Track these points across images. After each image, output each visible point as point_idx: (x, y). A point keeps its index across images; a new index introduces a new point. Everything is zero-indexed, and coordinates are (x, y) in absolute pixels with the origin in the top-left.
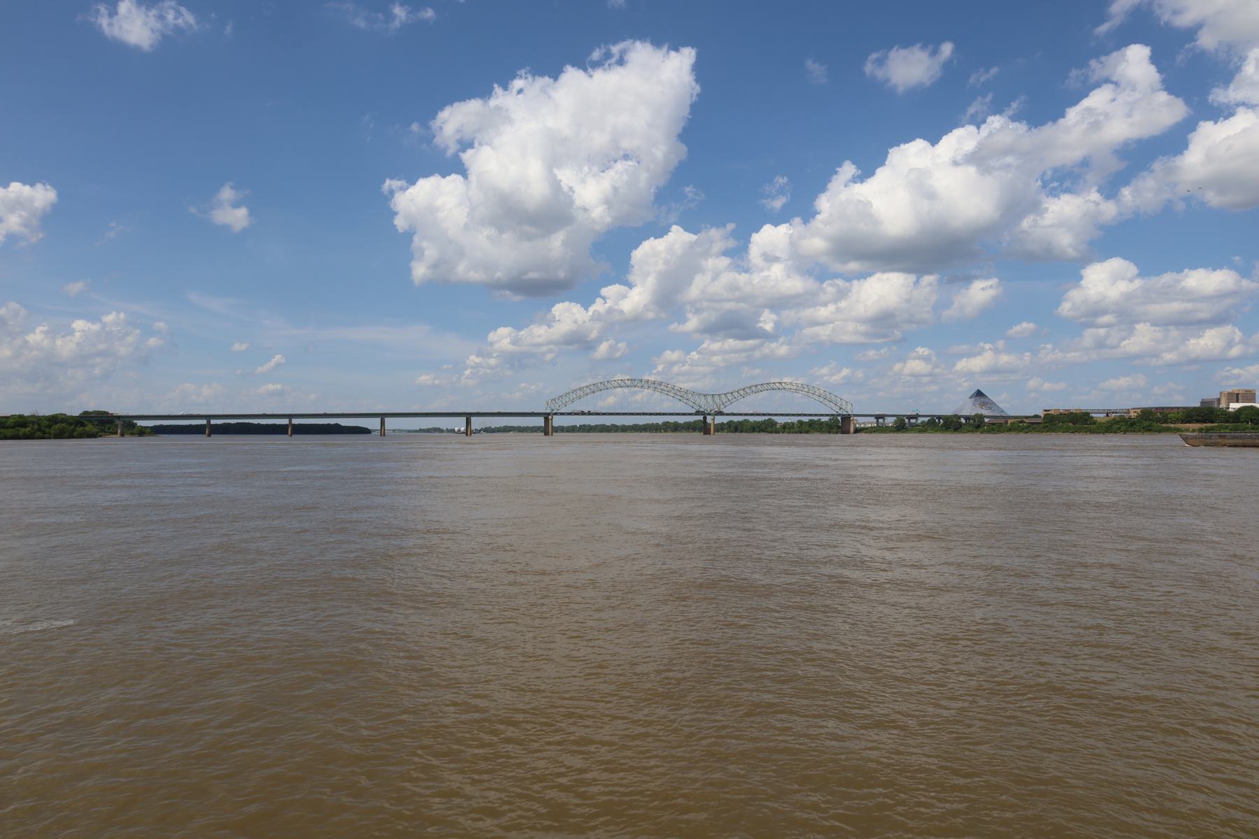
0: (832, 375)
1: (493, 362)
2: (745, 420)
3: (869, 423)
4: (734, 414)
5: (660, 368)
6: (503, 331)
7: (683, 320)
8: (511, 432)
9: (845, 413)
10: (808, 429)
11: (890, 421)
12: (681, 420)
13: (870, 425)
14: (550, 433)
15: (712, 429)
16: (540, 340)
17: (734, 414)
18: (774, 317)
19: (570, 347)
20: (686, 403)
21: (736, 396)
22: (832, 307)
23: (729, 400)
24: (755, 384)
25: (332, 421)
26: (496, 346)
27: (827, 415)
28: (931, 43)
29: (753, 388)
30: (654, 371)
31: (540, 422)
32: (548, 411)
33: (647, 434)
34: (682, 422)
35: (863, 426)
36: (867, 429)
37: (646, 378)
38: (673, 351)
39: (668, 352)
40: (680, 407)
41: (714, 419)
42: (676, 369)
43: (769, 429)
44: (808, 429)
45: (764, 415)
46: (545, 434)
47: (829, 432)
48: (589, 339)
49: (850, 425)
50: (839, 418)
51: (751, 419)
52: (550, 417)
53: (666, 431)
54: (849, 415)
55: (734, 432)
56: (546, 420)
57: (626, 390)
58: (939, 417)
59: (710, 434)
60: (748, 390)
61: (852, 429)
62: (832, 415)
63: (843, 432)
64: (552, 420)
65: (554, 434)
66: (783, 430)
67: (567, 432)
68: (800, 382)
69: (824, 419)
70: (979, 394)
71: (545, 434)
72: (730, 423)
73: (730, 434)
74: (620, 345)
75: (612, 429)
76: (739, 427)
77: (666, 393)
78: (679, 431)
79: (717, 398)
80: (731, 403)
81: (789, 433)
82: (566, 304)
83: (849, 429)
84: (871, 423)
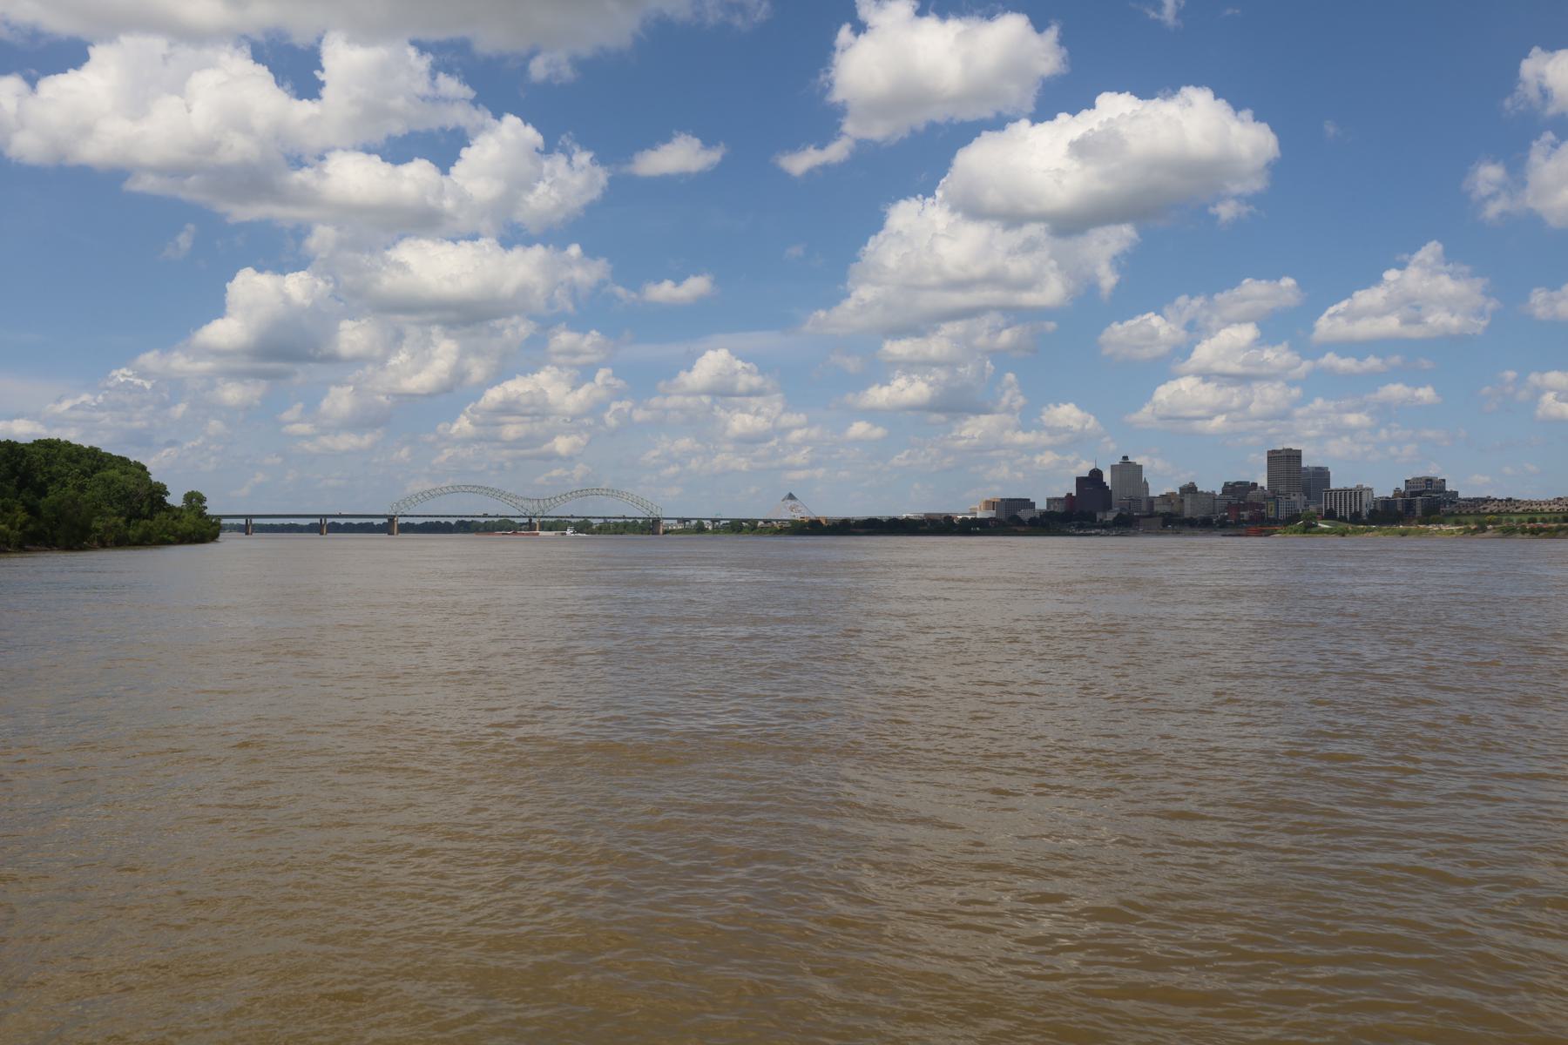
4: (430, 516)
12: (377, 522)
14: (395, 533)
17: (430, 516)
25: (293, 521)
28: (708, 143)
29: (574, 494)
33: (1217, 541)
45: (552, 517)
47: (642, 534)
50: (651, 521)
58: (746, 521)
61: (661, 531)
62: (644, 518)
70: (791, 497)
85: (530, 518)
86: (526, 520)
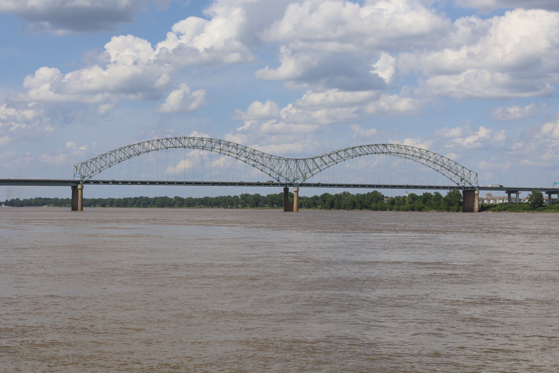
0: (464, 136)
1: (29, 114)
2: (344, 193)
3: (500, 199)
5: (248, 124)
6: (45, 72)
7: (276, 65)
8: (45, 207)
9: (467, 185)
10: (422, 205)
11: (524, 196)
12: (264, 192)
13: (501, 201)
14: (79, 208)
15: (295, 205)
16: (93, 86)
18: (392, 60)
19: (132, 97)
20: (262, 170)
21: (327, 161)
22: (464, 52)
23: (318, 167)
24: (351, 147)
26: (32, 93)
27: (444, 188)
30: (240, 129)
31: (66, 193)
32: (78, 178)
33: (221, 210)
34: (265, 195)
35: (492, 202)
36: (496, 206)
37: (229, 138)
38: (263, 102)
39: (257, 105)
40: (256, 175)
41: (297, 192)
42: (266, 126)
43: (373, 205)
44: (422, 205)
46: (73, 210)
47: (448, 210)
48: (409, 100)
49: (474, 201)
50: (461, 191)
51: (354, 192)
52: (79, 187)
53: (244, 206)
54: (473, 188)
55: (330, 209)
56: (75, 189)
57: (205, 152)
59: (292, 210)
60: (342, 154)
61: (476, 207)
62: (451, 188)
63: (465, 211)
64: (82, 189)
65: (84, 209)
66: (390, 206)
67: (118, 206)
68: (424, 147)
69: (444, 193)
71: (73, 210)
72: (325, 196)
73: (324, 210)
74: (196, 94)
75: (175, 203)
76: (336, 201)
77: (236, 156)
78: (261, 206)
79: (302, 165)
80: (321, 171)
81: (398, 210)
82: (130, 38)
83: (473, 206)
84: (501, 197)
85: (286, 186)
86: (279, 190)
